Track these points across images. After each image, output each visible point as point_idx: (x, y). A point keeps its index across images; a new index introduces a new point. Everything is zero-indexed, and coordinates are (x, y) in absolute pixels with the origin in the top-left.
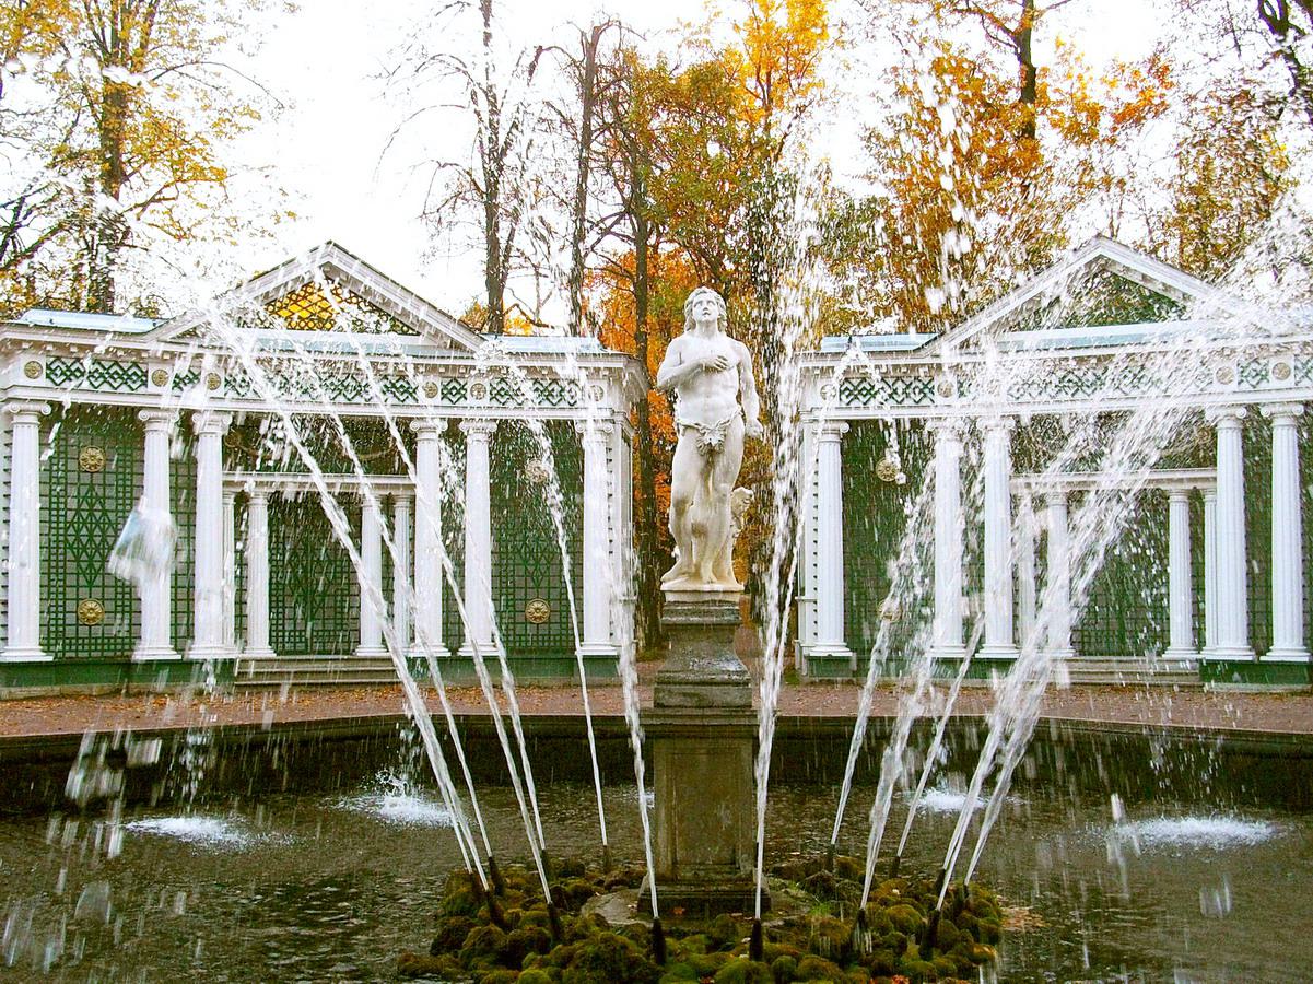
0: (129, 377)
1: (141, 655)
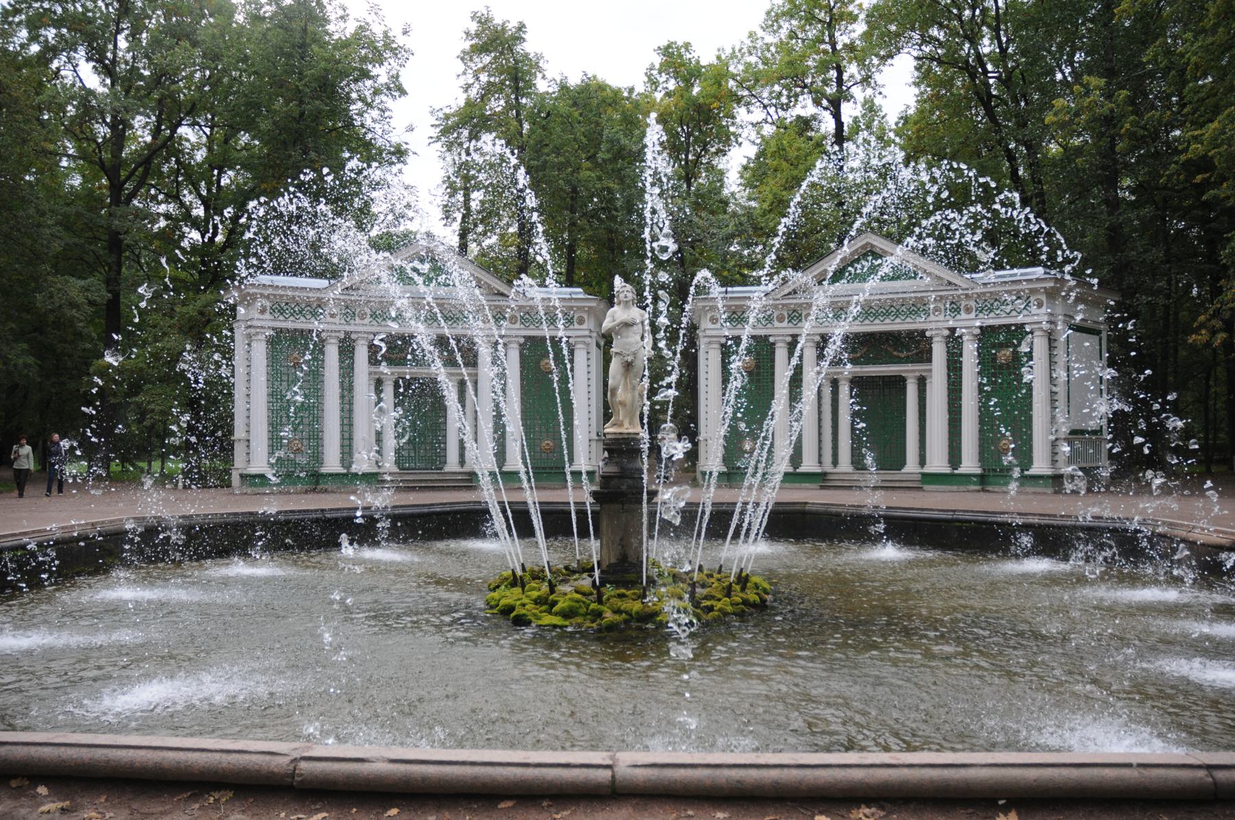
1: (324, 470)
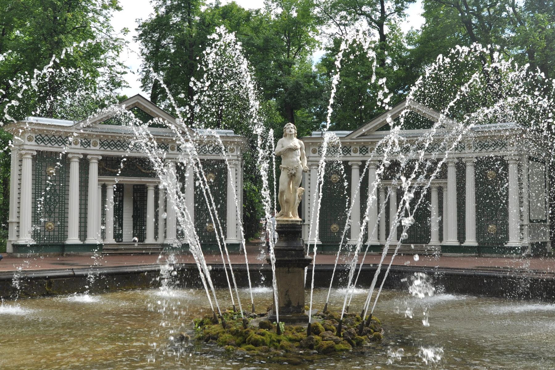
0: (117, 145)
1: (68, 242)
